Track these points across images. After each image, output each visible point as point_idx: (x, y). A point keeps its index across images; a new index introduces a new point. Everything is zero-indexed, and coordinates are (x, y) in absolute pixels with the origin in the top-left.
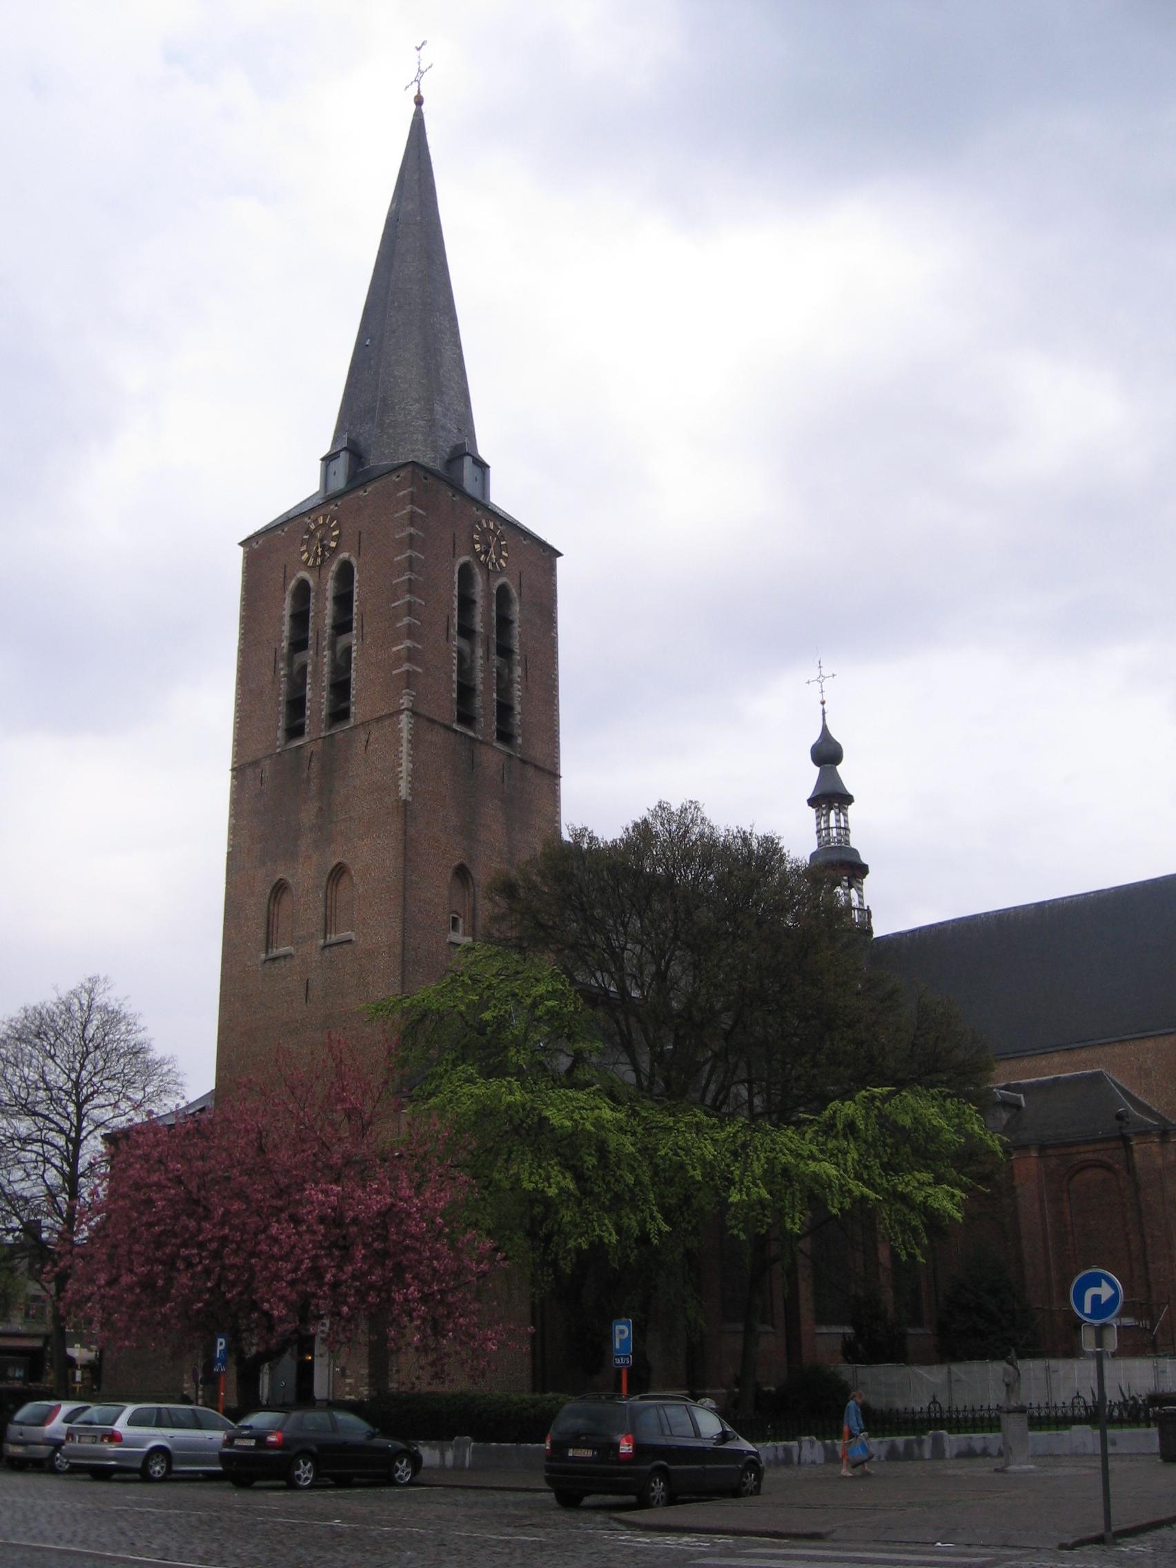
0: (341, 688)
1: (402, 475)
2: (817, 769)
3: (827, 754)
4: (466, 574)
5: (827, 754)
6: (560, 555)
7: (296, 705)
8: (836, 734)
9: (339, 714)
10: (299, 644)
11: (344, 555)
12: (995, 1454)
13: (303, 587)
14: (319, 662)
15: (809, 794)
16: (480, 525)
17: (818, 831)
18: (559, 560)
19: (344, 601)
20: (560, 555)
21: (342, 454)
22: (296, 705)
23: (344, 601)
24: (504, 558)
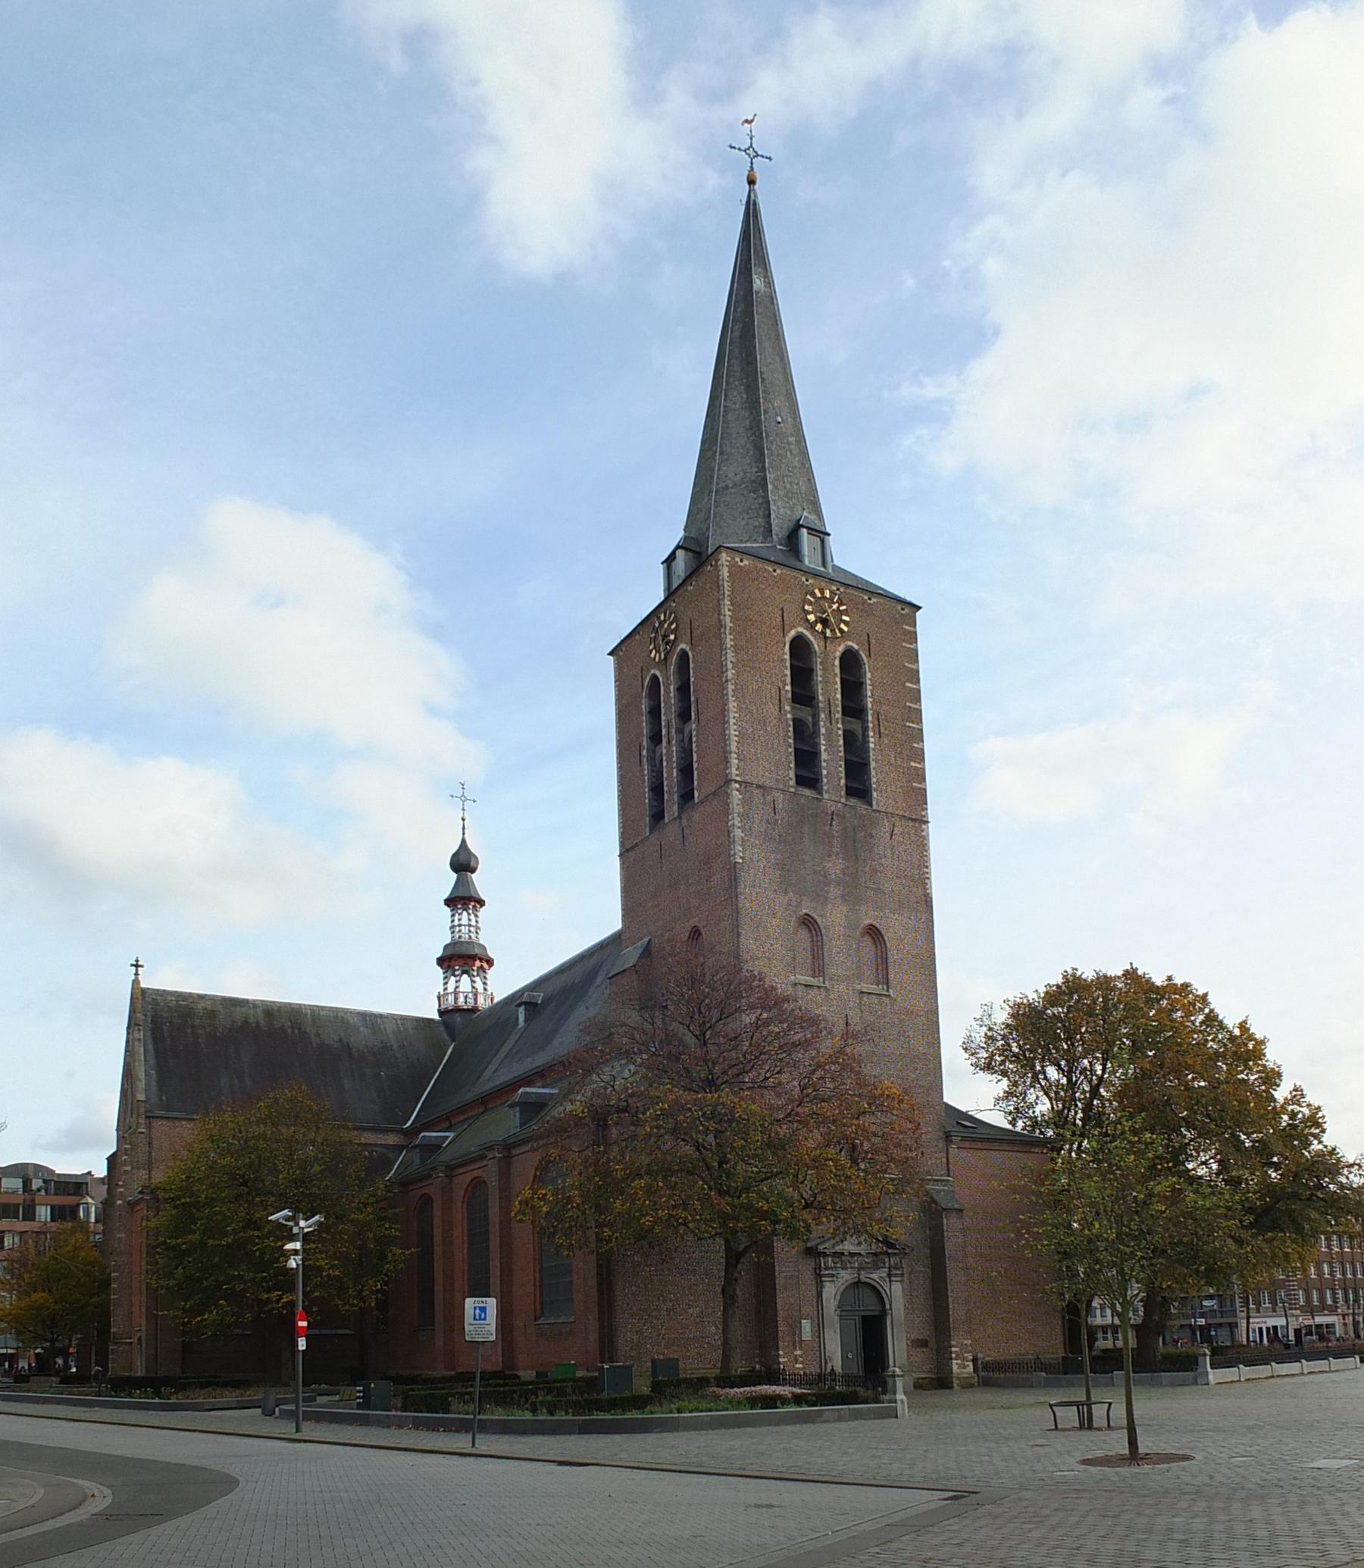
0: (686, 770)
1: (746, 562)
2: (455, 876)
3: (463, 863)
4: (800, 648)
5: (463, 863)
6: (919, 608)
7: (657, 790)
8: (472, 846)
9: (687, 796)
10: (656, 738)
11: (682, 646)
12: (642, 1386)
13: (655, 678)
14: (670, 753)
15: (446, 896)
16: (813, 594)
17: (452, 927)
18: (918, 614)
19: (684, 689)
20: (919, 608)
21: (680, 553)
22: (657, 790)
23: (684, 689)
24: (845, 622)
